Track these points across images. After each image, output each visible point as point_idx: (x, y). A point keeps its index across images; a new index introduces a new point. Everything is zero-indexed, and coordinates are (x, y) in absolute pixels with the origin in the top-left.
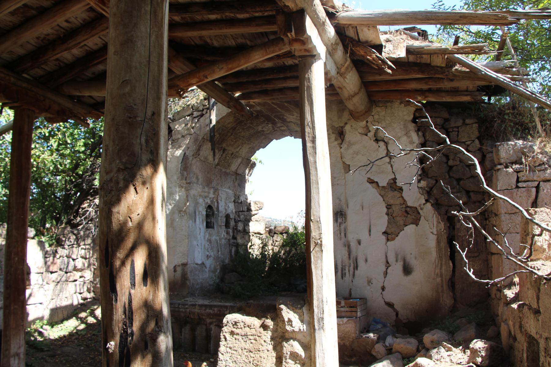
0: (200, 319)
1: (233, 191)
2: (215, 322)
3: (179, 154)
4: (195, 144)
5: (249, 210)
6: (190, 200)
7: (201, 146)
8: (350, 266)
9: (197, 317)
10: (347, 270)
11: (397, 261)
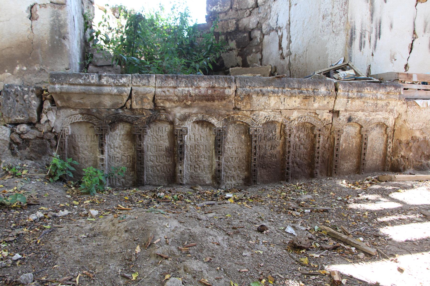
0: (156, 108)
2: (196, 114)
8: (371, 32)
9: (148, 106)
10: (367, 36)
11: (425, 31)
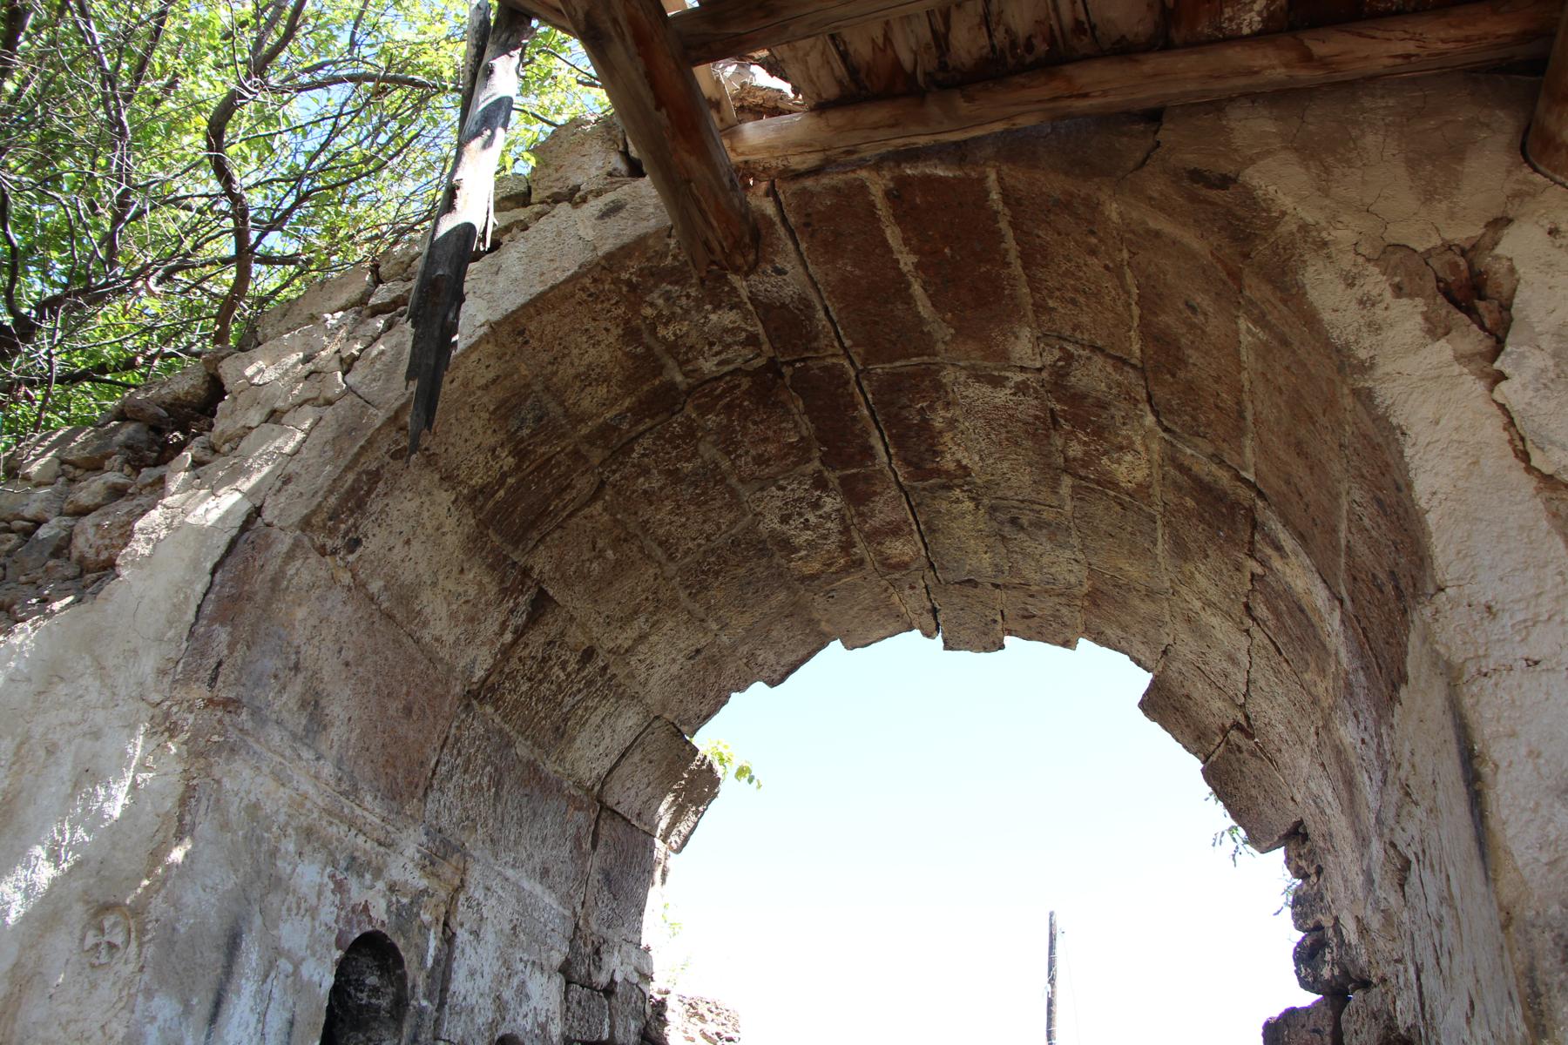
1: (566, 899)
3: (213, 516)
4: (340, 452)
6: (205, 827)
7: (375, 477)
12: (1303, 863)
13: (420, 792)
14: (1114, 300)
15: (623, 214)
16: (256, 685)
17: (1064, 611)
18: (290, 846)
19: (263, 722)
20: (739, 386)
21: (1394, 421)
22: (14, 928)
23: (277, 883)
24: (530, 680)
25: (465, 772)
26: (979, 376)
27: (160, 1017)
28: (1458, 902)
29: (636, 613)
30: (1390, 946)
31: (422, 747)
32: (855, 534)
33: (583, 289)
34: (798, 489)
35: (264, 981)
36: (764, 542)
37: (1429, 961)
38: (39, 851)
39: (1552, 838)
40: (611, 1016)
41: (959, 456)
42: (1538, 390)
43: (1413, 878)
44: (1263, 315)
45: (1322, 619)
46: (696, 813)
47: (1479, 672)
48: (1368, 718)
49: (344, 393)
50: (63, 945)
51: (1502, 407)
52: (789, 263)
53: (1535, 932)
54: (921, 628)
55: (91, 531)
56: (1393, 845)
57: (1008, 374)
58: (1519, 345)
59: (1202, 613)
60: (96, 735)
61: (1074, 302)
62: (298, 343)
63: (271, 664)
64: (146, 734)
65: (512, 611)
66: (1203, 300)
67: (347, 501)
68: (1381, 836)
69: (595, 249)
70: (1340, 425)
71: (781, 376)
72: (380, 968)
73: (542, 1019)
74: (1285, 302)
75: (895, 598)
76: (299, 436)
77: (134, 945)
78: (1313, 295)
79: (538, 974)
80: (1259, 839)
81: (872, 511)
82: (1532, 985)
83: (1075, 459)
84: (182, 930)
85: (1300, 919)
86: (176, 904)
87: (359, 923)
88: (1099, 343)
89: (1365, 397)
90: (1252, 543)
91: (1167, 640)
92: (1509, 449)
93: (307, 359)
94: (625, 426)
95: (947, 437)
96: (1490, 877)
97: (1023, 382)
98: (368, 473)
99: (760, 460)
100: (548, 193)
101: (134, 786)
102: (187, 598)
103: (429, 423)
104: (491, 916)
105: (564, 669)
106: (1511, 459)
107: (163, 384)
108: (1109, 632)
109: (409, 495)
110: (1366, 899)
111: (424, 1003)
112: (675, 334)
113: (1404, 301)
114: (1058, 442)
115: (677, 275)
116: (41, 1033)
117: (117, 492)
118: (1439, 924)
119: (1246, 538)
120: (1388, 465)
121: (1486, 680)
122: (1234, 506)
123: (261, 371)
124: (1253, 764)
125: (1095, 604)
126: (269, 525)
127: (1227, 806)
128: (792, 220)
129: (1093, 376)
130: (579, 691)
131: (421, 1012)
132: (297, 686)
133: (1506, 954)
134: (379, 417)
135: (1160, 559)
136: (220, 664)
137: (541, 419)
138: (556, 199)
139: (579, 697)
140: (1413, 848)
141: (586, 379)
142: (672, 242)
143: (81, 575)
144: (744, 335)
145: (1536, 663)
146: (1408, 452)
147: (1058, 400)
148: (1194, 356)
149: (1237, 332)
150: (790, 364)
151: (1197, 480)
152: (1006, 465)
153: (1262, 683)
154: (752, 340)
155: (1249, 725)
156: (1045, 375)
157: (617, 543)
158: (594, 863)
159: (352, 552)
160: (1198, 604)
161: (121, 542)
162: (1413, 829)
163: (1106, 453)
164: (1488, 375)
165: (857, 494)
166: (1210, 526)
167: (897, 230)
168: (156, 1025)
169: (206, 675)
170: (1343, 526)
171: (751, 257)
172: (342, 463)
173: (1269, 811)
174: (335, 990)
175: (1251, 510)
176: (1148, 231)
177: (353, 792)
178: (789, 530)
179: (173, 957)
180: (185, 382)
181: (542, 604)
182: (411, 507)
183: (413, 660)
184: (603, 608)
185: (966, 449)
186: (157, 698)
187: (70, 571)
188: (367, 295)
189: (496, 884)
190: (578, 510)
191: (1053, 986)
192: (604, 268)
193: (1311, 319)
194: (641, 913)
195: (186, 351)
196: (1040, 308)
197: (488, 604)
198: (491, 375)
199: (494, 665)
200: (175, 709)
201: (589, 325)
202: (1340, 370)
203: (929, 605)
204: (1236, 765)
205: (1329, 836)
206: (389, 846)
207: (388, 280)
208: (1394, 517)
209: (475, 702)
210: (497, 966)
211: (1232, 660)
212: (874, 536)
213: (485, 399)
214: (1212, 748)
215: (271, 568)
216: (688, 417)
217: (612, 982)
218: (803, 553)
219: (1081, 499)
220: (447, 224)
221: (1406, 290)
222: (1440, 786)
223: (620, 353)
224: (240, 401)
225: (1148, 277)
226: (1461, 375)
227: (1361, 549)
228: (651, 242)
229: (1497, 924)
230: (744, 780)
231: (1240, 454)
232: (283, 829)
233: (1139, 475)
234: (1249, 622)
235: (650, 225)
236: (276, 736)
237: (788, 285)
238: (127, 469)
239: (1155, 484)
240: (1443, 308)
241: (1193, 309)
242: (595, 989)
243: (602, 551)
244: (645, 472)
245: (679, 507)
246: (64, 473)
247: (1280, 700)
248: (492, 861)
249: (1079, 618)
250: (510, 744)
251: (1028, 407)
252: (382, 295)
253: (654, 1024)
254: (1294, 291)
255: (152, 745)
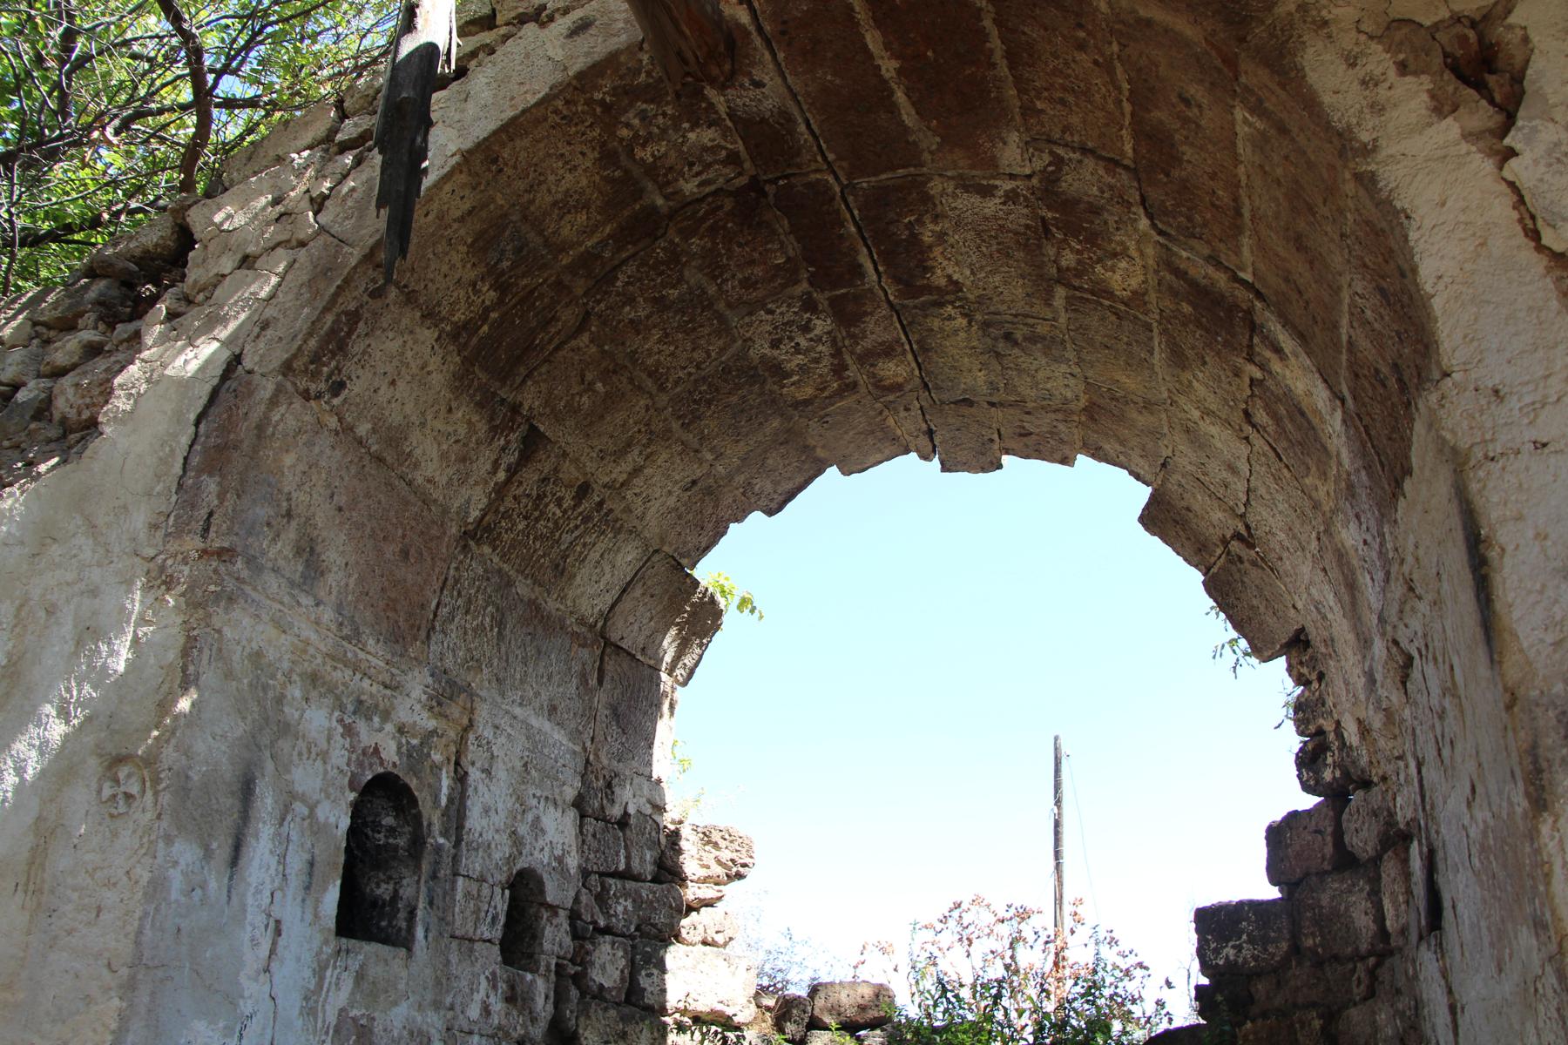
1: (575, 735)
3: (193, 366)
4: (316, 294)
5: (669, 872)
6: (210, 676)
7: (354, 317)
12: (1305, 670)
13: (423, 634)
14: (1104, 97)
15: (592, 31)
16: (249, 534)
17: (1061, 427)
18: (296, 692)
19: (260, 569)
20: (722, 207)
21: (1398, 205)
22: (33, 784)
23: (286, 729)
24: (526, 518)
25: (467, 612)
26: (968, 186)
27: (182, 862)
28: (1462, 692)
29: (629, 445)
30: (1390, 745)
31: (422, 589)
32: (848, 359)
33: (556, 112)
34: (786, 312)
35: (281, 825)
36: (756, 368)
37: (1430, 753)
38: (49, 709)
39: (1558, 618)
40: (626, 847)
41: (950, 271)
42: (1551, 165)
43: (1416, 674)
44: (1260, 101)
45: (1323, 421)
46: (700, 645)
47: (1486, 457)
48: (1370, 518)
49: (317, 234)
50: (81, 798)
51: (1511, 184)
52: (766, 73)
53: (1539, 711)
54: (917, 451)
55: (70, 392)
56: (1396, 642)
57: (998, 183)
58: (1531, 119)
59: (1201, 423)
60: (94, 592)
61: (1062, 102)
62: (266, 185)
63: (263, 512)
64: (143, 589)
65: (503, 449)
66: (1196, 91)
67: (328, 343)
68: (1383, 634)
69: (566, 69)
70: (1341, 212)
71: (765, 195)
72: (395, 808)
73: (558, 852)
74: (1283, 86)
75: (891, 422)
76: (274, 280)
77: (149, 793)
78: (1312, 78)
79: (552, 809)
80: (1262, 650)
81: (864, 331)
82: (1535, 762)
83: (1068, 269)
84: (196, 778)
85: (1302, 726)
86: (188, 753)
87: (371, 765)
88: (1090, 145)
89: (1368, 182)
90: (1250, 346)
91: (1166, 453)
92: (1519, 228)
93: (276, 202)
94: (607, 254)
95: (937, 251)
96: (1495, 656)
97: (1013, 190)
98: (346, 313)
99: (747, 284)
100: (513, 14)
101: (136, 640)
102: (172, 451)
103: (403, 251)
104: (502, 754)
105: (559, 506)
106: (1521, 239)
107: (131, 238)
108: (1107, 447)
109: (391, 335)
110: (1368, 699)
111: (441, 840)
112: (653, 155)
113: (1408, 79)
114: (1051, 251)
115: (652, 93)
116: (69, 880)
117: (93, 351)
118: (1442, 716)
119: (1245, 342)
120: (1391, 251)
121: (1492, 465)
122: (1233, 308)
123: (229, 217)
124: (1254, 573)
125: (1092, 418)
126: (249, 372)
127: (1230, 617)
128: (767, 28)
129: (1085, 179)
130: (577, 527)
131: (438, 849)
132: (291, 534)
133: (1510, 734)
134: (354, 255)
135: (1157, 369)
136: (211, 514)
137: (520, 250)
138: (522, 20)
139: (577, 533)
140: (1416, 643)
141: (564, 206)
142: (645, 58)
143: (64, 436)
144: (724, 153)
145: (1544, 445)
146: (1413, 236)
147: (1049, 208)
148: (1188, 153)
149: (1233, 123)
150: (774, 181)
151: (1193, 283)
152: (997, 278)
153: (1262, 491)
154: (733, 159)
155: (1250, 535)
156: (1035, 181)
157: (605, 375)
158: (601, 699)
159: (336, 395)
160: (1196, 414)
161: (101, 399)
162: (1416, 624)
163: (1099, 260)
164: (1497, 152)
165: (848, 315)
166: (1207, 331)
167: (877, 34)
168: (179, 869)
169: (199, 526)
170: (1345, 321)
171: (727, 67)
172: (320, 304)
173: (1271, 620)
174: (353, 832)
175: (1249, 312)
176: (1139, 20)
177: (355, 637)
178: (781, 354)
179: (189, 804)
180: (154, 234)
181: (533, 442)
182: (394, 346)
183: (407, 503)
184: (595, 442)
185: (957, 263)
186: (151, 552)
187: (53, 432)
188: (334, 131)
189: (504, 722)
190: (564, 343)
191: (1059, 807)
192: (576, 88)
193: (1310, 103)
194: (650, 746)
195: (151, 204)
196: (1028, 111)
197: (478, 443)
198: (467, 206)
199: (490, 504)
200: (169, 562)
201: (565, 150)
202: (1342, 153)
203: (924, 427)
204: (1237, 576)
205: (1330, 642)
206: (395, 689)
207: (354, 114)
208: (1398, 307)
209: (472, 543)
210: (510, 802)
211: (1232, 469)
212: (866, 358)
213: (462, 232)
214: (1213, 560)
215: (255, 416)
216: (671, 242)
217: (626, 814)
218: (795, 378)
219: (1075, 310)
220: (408, 46)
221: (1412, 67)
222: (1444, 577)
223: (597, 178)
224: (211, 248)
225: (1140, 70)
226: (1468, 153)
227: (1364, 343)
228: (623, 58)
229: (1502, 705)
230: (747, 611)
231: (1238, 253)
232: (288, 675)
233: (1134, 283)
234: (1248, 429)
235: (620, 41)
236: (272, 582)
237: (766, 98)
238: (102, 326)
239: (1151, 292)
240: (1451, 84)
241: (1187, 102)
242: (609, 822)
243: (592, 384)
244: (631, 301)
245: (667, 335)
246: (38, 335)
247: (1281, 507)
248: (499, 699)
249: (1077, 434)
250: (510, 583)
251: (1019, 216)
252: (349, 130)
253: (669, 853)
254: (1293, 74)
255: (150, 600)
